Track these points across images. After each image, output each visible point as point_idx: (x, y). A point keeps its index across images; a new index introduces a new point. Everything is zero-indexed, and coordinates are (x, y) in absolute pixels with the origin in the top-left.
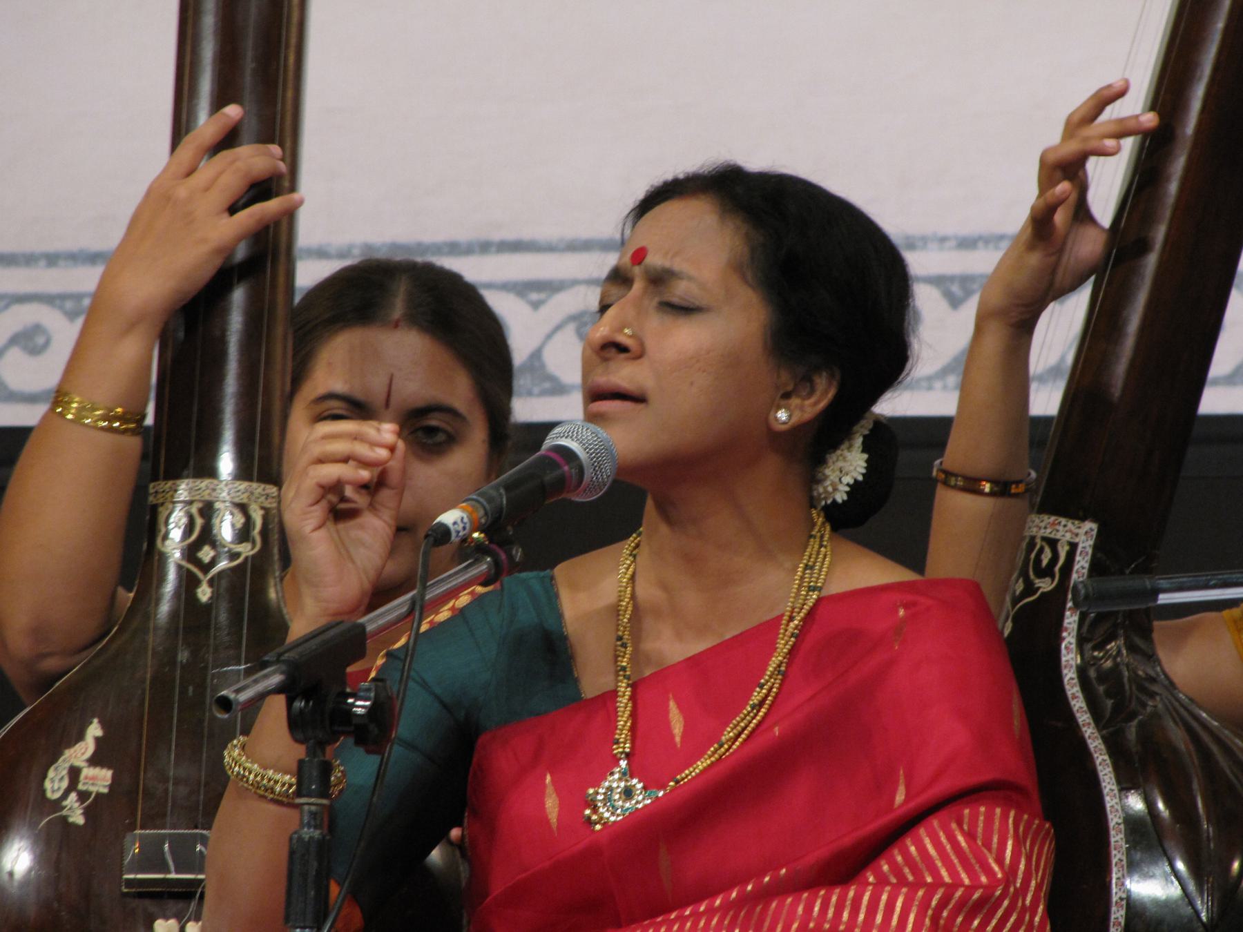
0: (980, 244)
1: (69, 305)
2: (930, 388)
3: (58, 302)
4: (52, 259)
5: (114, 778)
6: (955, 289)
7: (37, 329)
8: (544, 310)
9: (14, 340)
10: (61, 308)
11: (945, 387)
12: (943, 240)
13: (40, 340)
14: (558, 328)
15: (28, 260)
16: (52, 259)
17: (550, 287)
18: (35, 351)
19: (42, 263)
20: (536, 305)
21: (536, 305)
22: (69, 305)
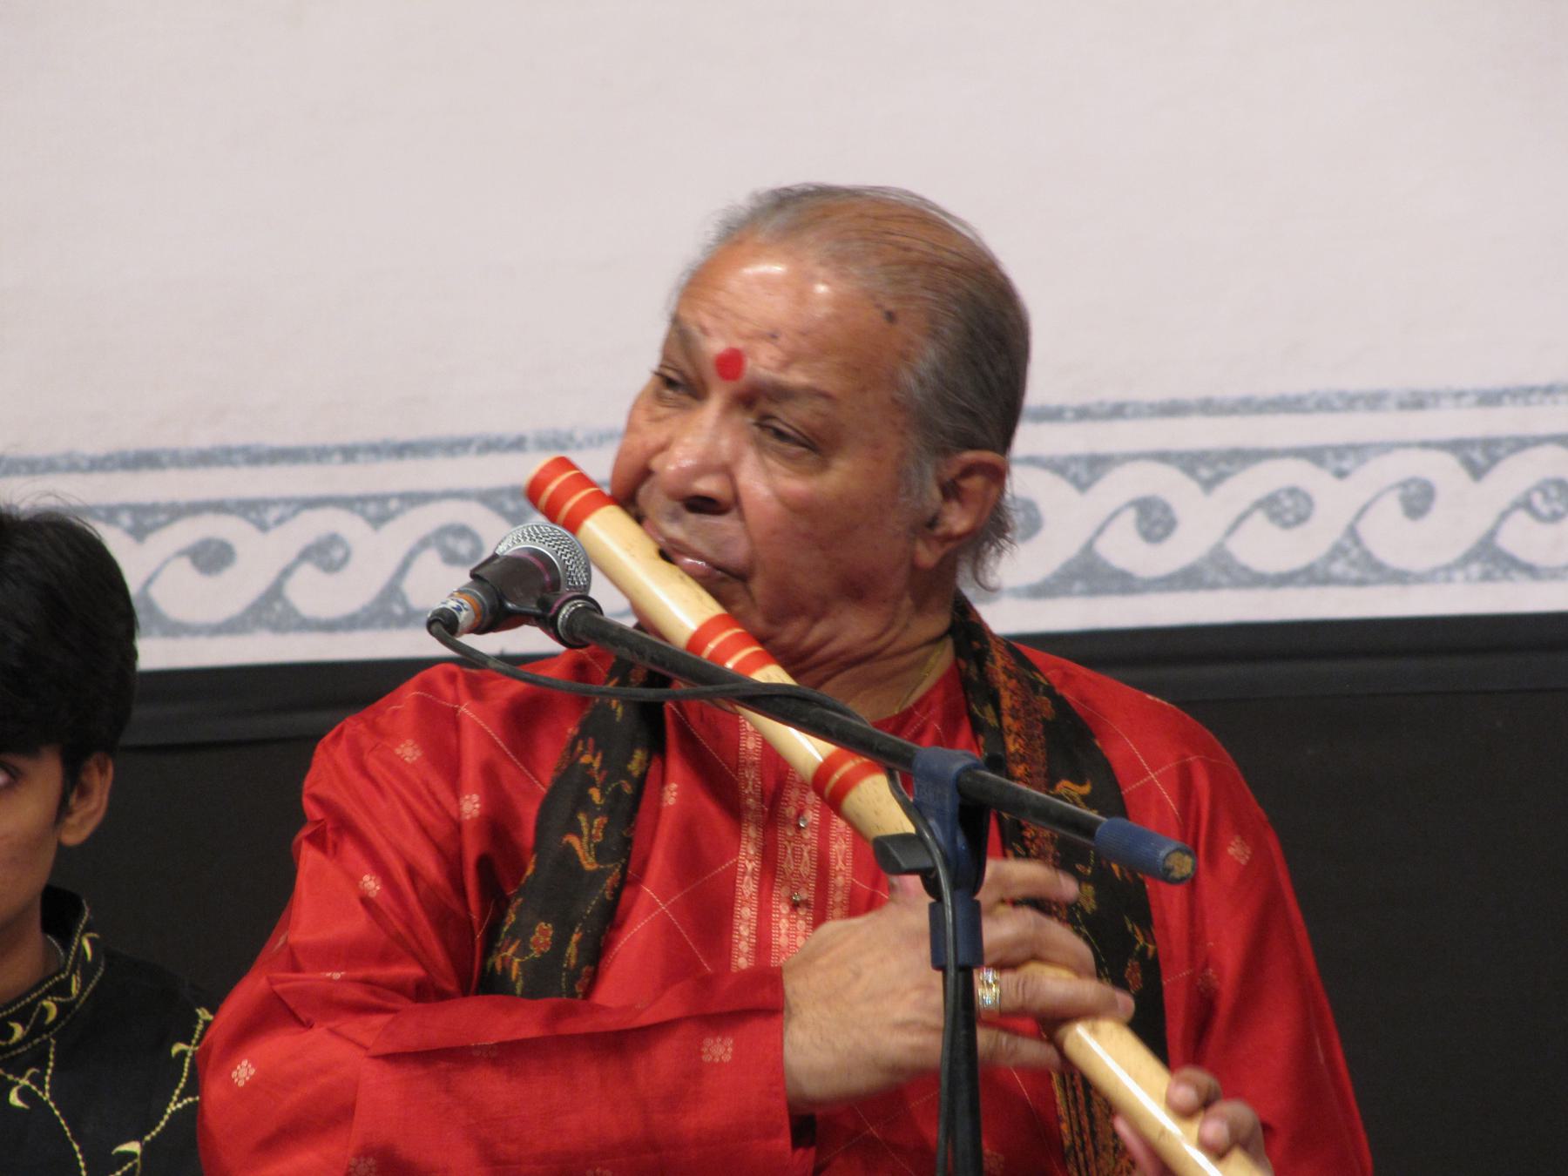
0: (1507, 399)
1: (372, 509)
2: (1449, 580)
3: (358, 506)
4: (349, 453)
5: (132, 655)
6: (1477, 456)
7: (333, 540)
8: (1223, 490)
9: (305, 555)
10: (363, 513)
11: (1468, 579)
12: (1459, 395)
13: (337, 554)
14: (1242, 518)
15: (320, 454)
16: (349, 453)
17: (1360, 451)
18: (332, 567)
19: (337, 458)
20: (1208, 485)
21: (1208, 485)
22: (372, 509)
